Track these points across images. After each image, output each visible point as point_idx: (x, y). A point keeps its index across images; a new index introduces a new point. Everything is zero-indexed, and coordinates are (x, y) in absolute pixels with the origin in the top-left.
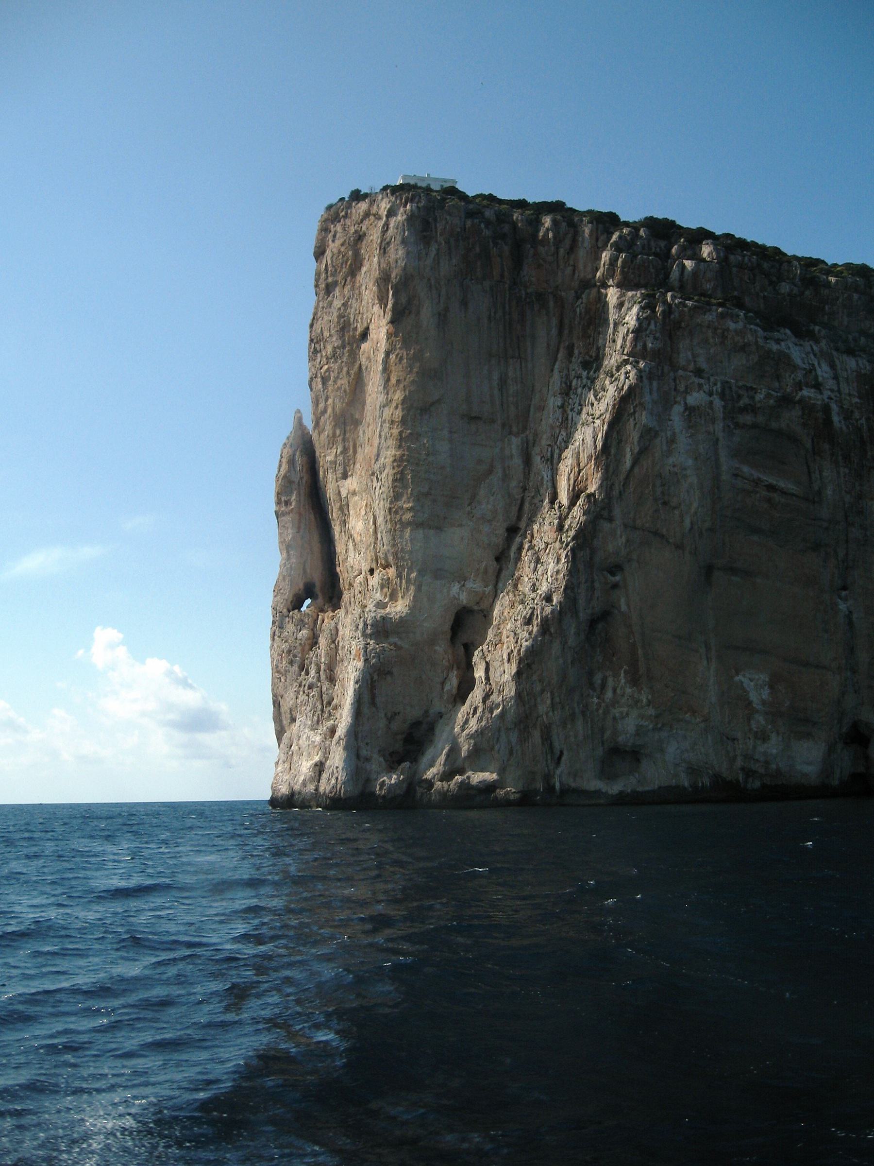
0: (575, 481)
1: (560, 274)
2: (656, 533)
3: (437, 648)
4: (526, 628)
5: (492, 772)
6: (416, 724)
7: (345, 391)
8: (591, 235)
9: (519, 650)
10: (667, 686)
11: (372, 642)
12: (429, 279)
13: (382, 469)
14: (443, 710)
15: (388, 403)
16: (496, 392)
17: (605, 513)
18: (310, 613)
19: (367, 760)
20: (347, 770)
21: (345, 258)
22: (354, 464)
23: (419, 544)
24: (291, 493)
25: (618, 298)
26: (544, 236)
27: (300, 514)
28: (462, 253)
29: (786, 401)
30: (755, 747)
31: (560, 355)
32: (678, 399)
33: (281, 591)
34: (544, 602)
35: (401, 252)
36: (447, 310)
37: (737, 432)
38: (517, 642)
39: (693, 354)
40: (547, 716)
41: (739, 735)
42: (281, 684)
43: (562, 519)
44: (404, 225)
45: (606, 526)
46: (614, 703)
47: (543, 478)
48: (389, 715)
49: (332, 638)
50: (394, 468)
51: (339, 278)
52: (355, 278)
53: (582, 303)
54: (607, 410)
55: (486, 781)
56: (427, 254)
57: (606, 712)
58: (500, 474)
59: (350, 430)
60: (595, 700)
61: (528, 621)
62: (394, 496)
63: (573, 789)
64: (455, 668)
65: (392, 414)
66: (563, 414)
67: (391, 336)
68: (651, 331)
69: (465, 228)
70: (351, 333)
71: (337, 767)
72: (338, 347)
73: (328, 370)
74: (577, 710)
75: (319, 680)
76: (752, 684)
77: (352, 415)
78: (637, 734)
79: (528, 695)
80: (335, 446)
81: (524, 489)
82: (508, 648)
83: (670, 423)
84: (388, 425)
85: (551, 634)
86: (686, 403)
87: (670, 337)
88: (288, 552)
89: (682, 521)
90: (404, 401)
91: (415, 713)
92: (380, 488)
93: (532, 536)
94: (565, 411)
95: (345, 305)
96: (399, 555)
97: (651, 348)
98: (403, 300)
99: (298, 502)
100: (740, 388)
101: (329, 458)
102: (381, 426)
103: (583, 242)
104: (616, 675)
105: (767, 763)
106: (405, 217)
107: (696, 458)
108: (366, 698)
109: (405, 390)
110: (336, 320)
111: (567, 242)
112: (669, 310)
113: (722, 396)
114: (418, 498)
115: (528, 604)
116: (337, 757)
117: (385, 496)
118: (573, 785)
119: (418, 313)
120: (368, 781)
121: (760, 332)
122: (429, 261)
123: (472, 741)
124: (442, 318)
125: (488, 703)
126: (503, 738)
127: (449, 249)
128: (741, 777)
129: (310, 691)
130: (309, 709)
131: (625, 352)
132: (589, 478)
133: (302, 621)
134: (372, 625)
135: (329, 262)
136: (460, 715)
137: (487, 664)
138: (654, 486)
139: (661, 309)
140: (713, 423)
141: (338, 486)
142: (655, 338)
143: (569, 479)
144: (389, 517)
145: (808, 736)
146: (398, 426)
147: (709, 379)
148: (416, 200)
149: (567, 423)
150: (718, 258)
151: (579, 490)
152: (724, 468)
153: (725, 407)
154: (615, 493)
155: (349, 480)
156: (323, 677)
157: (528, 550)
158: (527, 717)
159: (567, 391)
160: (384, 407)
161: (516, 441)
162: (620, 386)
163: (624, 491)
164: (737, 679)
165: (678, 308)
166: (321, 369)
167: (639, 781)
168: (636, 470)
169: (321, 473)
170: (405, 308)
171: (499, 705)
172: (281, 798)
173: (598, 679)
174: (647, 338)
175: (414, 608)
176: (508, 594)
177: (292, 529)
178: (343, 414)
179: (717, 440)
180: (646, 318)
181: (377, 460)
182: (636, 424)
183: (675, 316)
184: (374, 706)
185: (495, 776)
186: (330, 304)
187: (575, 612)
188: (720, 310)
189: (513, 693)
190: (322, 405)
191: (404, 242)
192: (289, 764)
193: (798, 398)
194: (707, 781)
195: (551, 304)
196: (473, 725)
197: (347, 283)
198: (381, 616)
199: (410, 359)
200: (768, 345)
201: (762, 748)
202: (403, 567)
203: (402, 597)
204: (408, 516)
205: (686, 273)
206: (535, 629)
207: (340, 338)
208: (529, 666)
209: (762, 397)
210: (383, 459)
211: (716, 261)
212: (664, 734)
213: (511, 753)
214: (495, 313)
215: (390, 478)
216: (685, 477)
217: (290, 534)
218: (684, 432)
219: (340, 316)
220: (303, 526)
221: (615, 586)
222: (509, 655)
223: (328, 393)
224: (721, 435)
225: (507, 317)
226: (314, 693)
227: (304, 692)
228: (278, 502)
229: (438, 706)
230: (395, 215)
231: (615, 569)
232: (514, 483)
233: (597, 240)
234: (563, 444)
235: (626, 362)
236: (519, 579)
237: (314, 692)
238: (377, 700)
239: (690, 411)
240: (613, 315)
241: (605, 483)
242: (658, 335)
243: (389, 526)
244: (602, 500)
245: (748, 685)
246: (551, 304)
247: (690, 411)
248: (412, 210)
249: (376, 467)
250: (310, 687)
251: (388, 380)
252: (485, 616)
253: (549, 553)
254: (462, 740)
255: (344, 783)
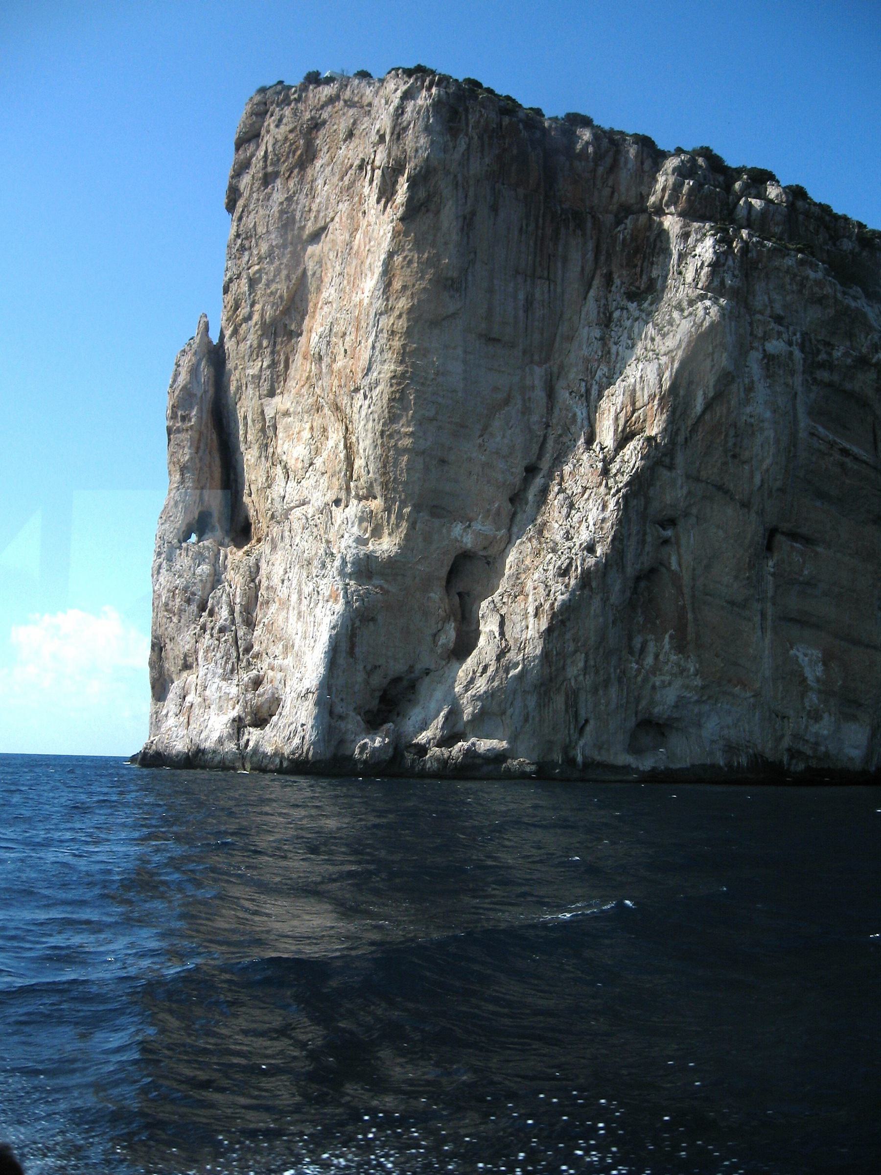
0: (626, 422)
1: (596, 193)
2: (720, 488)
3: (432, 595)
4: (560, 579)
5: (501, 740)
6: (397, 680)
7: (281, 297)
8: (636, 157)
9: (552, 604)
10: (717, 656)
11: (352, 583)
12: (455, 176)
13: (373, 386)
14: (433, 667)
15: (388, 311)
16: (521, 313)
17: (667, 460)
18: (210, 546)
19: (341, 717)
20: (317, 728)
21: (294, 147)
22: (285, 381)
23: (417, 475)
24: (191, 408)
25: (681, 228)
26: (582, 150)
27: (201, 433)
28: (497, 152)
29: (863, 362)
30: (807, 727)
31: (596, 282)
32: (755, 344)
33: (172, 519)
34: (585, 552)
35: (423, 141)
36: (473, 213)
37: (814, 388)
38: (548, 595)
39: (769, 298)
40: (576, 680)
41: (791, 713)
42: (172, 625)
43: (607, 462)
44: (428, 111)
45: (665, 474)
46: (656, 670)
47: (575, 415)
48: (369, 667)
49: (251, 576)
50: (391, 386)
51: (283, 168)
52: (305, 171)
53: (625, 229)
54: (679, 347)
55: (494, 749)
56: (454, 148)
57: (645, 680)
58: (519, 406)
59: (282, 342)
60: (635, 666)
61: (564, 572)
62: (389, 417)
63: (598, 762)
64: (452, 619)
65: (393, 324)
66: (603, 347)
67: (399, 235)
68: (729, 267)
69: (501, 125)
70: (296, 232)
71: (303, 725)
72: (277, 246)
73: (259, 271)
74: (612, 676)
75: (233, 622)
76: (806, 659)
77: (285, 326)
78: (676, 706)
79: (557, 655)
80: (260, 359)
81: (548, 426)
82: (536, 600)
83: (747, 370)
84: (386, 336)
85: (591, 589)
86: (764, 350)
87: (746, 276)
88: (182, 474)
89: (752, 477)
90: (410, 311)
91: (397, 667)
92: (369, 407)
93: (562, 479)
94: (605, 344)
95: (289, 199)
96: (390, 486)
97: (731, 286)
98: (422, 194)
99: (200, 418)
100: (818, 341)
101: (251, 372)
102: (376, 336)
103: (626, 163)
104: (659, 640)
105: (817, 744)
106: (429, 102)
107: (775, 411)
108: (344, 646)
109: (412, 298)
110: (277, 215)
111: (608, 160)
112: (746, 248)
113: (802, 349)
114: (421, 422)
115: (562, 553)
116: (304, 713)
117: (376, 416)
118: (598, 758)
119: (438, 212)
120: (342, 742)
121: (838, 287)
122: (457, 156)
123: (479, 704)
124: (468, 223)
125: (504, 661)
126: (518, 703)
127: (482, 146)
128: (785, 759)
129: (222, 635)
130: (219, 655)
131: (700, 286)
132: (648, 419)
133: (201, 554)
134: (353, 563)
135: (270, 149)
136: (461, 673)
137: (503, 617)
138: (726, 436)
139: (739, 245)
140: (793, 375)
141: (262, 404)
142: (734, 276)
143: (617, 418)
144: (379, 441)
145: (853, 718)
146: (400, 337)
147: (788, 328)
148: (444, 84)
149: (609, 358)
150: (787, 202)
151: (631, 431)
152: (802, 425)
153: (805, 360)
154: (680, 439)
155: (277, 399)
156: (238, 619)
157: (558, 493)
158: (551, 680)
159: (606, 321)
160: (381, 314)
161: (539, 371)
162: (698, 321)
163: (691, 437)
164: (792, 652)
165: (756, 247)
166: (249, 269)
167: (668, 757)
168: (707, 417)
169: (232, 388)
170: (422, 205)
171: (518, 664)
172: (177, 756)
173: (637, 642)
174: (726, 275)
175: (407, 546)
176: (530, 540)
177: (190, 448)
178: (274, 322)
179: (796, 393)
180: (723, 253)
181: (367, 374)
182: (713, 366)
183: (753, 254)
184: (352, 657)
185: (504, 744)
186: (268, 197)
187: (622, 568)
188: (799, 256)
189: (538, 651)
190: (243, 311)
191: (427, 129)
192: (186, 717)
193: (874, 361)
194: (744, 760)
195: (589, 225)
196: (481, 685)
197: (293, 175)
198: (365, 554)
199: (422, 263)
200: (847, 301)
201: (815, 728)
202: (394, 500)
203: (389, 534)
204: (407, 442)
205: (753, 213)
206: (573, 582)
207: (281, 236)
208: (563, 622)
209: (839, 354)
210: (375, 374)
211: (785, 204)
212: (706, 708)
213: (526, 720)
214: (527, 225)
215: (386, 397)
216: (762, 430)
217: (185, 456)
218: (762, 381)
219: (282, 212)
220: (202, 446)
221: (666, 542)
222: (537, 609)
223: (256, 298)
224: (800, 389)
225: (540, 231)
226: (226, 637)
227: (212, 636)
228: (174, 416)
229: (426, 661)
230: (414, 98)
231: (671, 522)
232: (535, 418)
233: (642, 163)
234: (604, 380)
235: (702, 298)
236: (545, 524)
237: (228, 636)
238: (357, 650)
239: (769, 359)
240: (675, 247)
241: (670, 426)
242: (737, 272)
243: (379, 452)
244: (665, 444)
245: (804, 660)
246: (589, 225)
247: (769, 359)
248: (439, 95)
249: (366, 382)
250: (222, 630)
251: (389, 285)
252: (488, 563)
253: (588, 499)
254: (464, 701)
255: (313, 743)
